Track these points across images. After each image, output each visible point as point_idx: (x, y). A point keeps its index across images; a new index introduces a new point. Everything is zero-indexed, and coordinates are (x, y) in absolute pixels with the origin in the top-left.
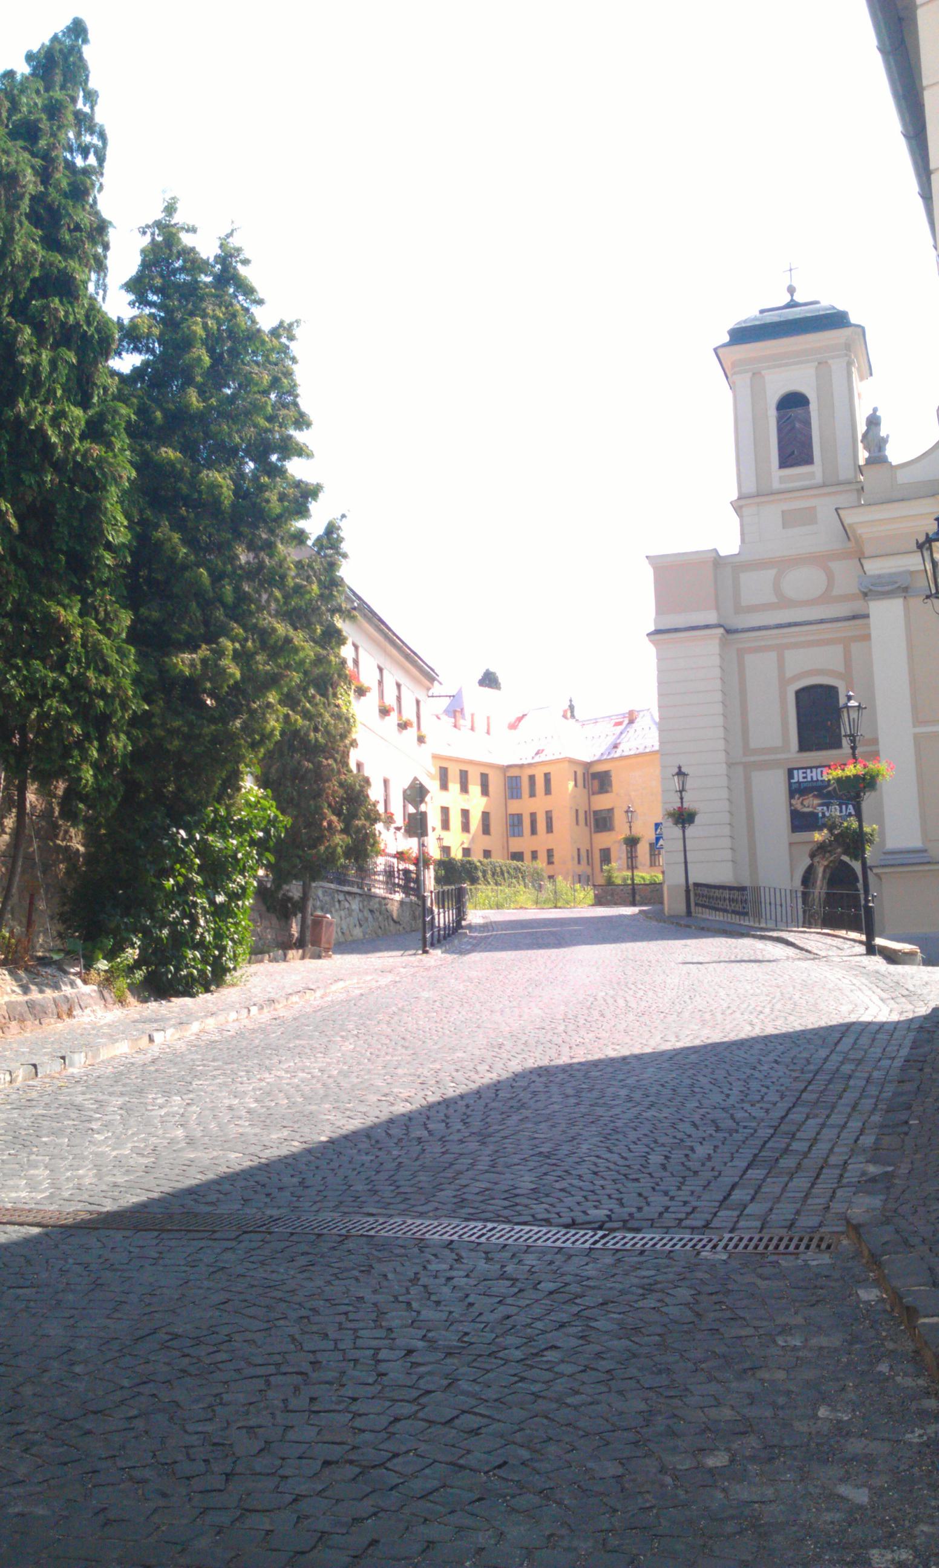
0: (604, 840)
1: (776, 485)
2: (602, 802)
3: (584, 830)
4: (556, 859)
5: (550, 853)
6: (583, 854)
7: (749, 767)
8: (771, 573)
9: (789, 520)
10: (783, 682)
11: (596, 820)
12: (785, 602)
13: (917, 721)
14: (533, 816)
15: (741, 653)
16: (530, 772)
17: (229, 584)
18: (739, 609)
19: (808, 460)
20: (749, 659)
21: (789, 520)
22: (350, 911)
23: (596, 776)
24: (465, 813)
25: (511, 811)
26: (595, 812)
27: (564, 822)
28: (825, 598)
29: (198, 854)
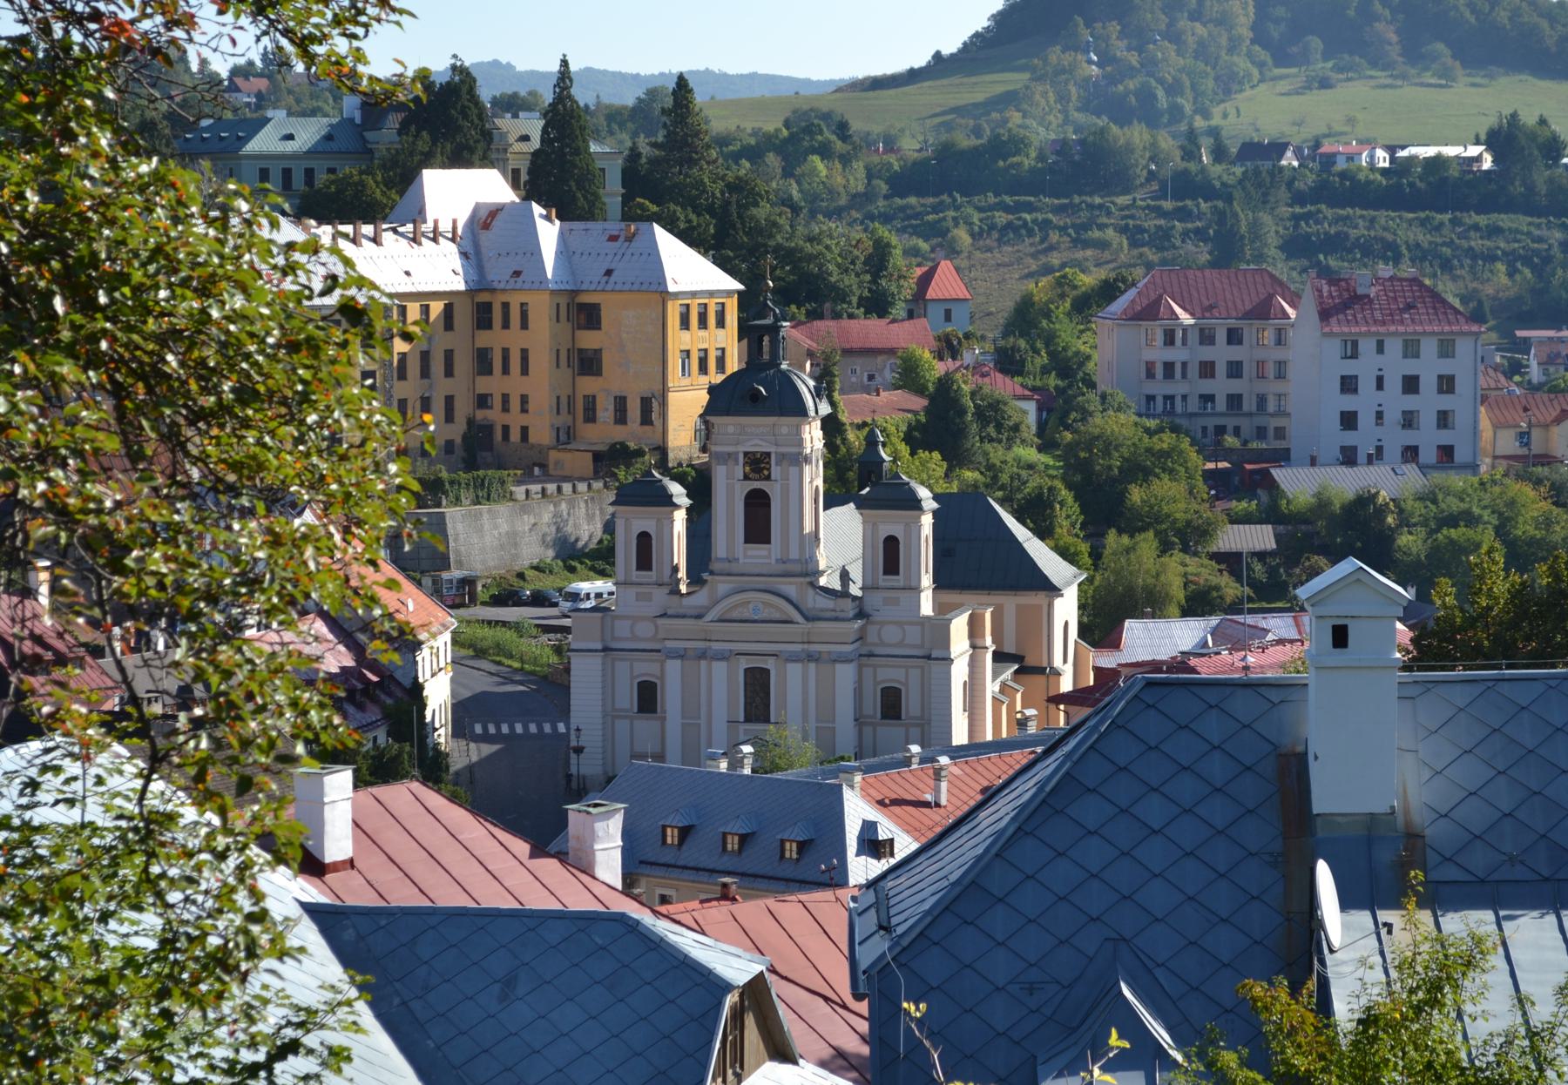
0: (587, 385)
1: (634, 579)
2: (589, 340)
3: (565, 373)
4: (531, 406)
5: (524, 400)
6: (564, 401)
7: (614, 717)
8: (629, 622)
9: (639, 597)
10: (632, 678)
11: (582, 360)
12: (634, 638)
13: (683, 717)
14: (506, 353)
15: (613, 660)
16: (505, 298)
17: (134, 167)
18: (614, 639)
19: (650, 569)
20: (617, 663)
22: (262, 480)
23: (583, 307)
24: (449, 356)
25: (479, 344)
26: (580, 351)
27: (541, 361)
29: (65, 458)
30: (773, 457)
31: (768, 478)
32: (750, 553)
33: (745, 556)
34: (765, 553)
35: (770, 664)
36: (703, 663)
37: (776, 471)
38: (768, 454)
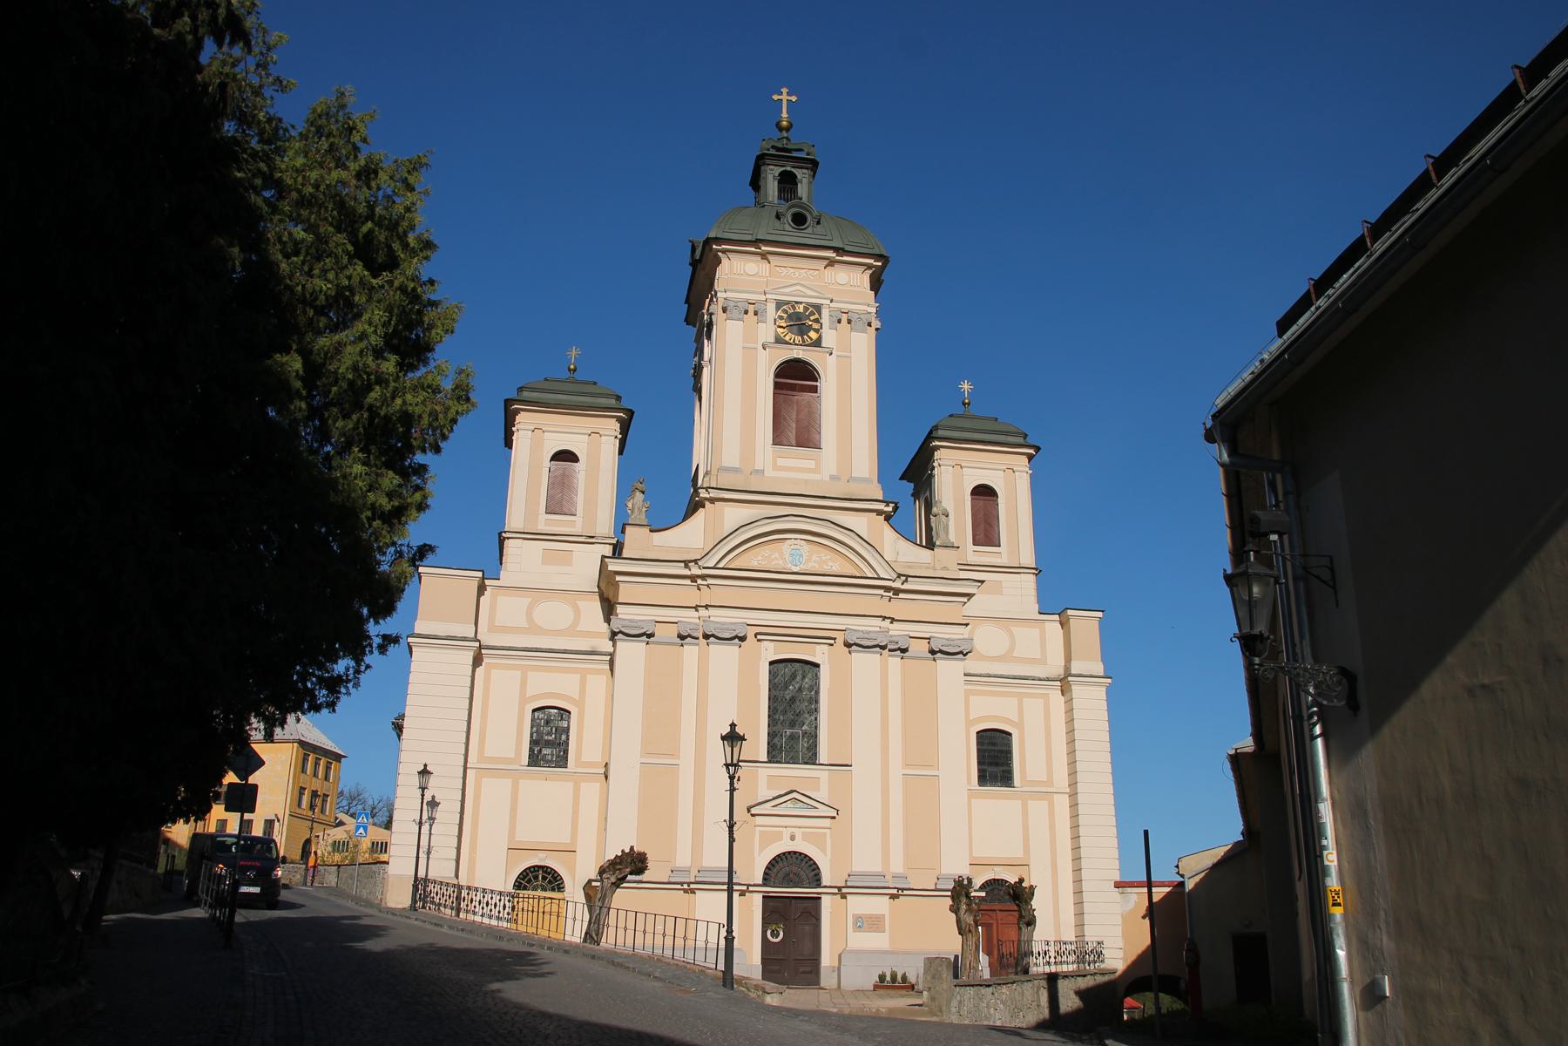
9: (548, 558)
10: (523, 700)
21: (548, 558)
28: (571, 631)
30: (825, 312)
31: (817, 343)
32: (781, 462)
33: (776, 468)
34: (812, 464)
35: (818, 654)
36: (691, 651)
37: (829, 337)
38: (818, 308)
